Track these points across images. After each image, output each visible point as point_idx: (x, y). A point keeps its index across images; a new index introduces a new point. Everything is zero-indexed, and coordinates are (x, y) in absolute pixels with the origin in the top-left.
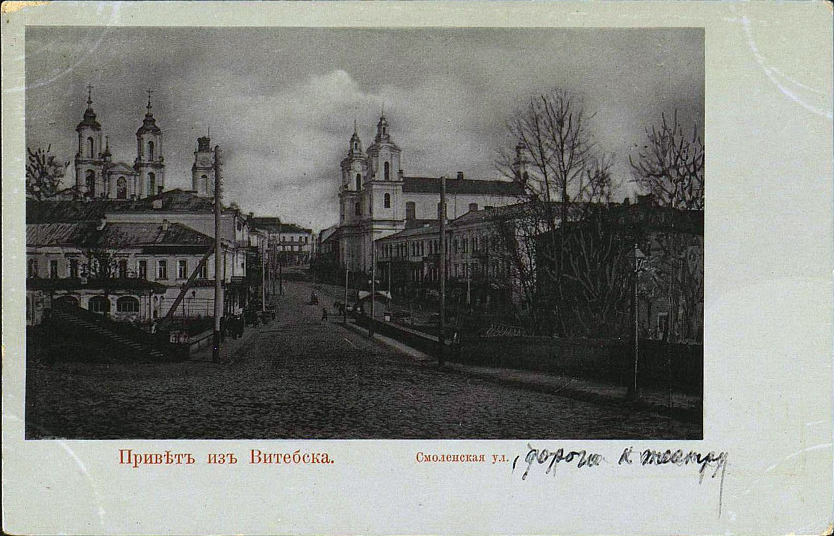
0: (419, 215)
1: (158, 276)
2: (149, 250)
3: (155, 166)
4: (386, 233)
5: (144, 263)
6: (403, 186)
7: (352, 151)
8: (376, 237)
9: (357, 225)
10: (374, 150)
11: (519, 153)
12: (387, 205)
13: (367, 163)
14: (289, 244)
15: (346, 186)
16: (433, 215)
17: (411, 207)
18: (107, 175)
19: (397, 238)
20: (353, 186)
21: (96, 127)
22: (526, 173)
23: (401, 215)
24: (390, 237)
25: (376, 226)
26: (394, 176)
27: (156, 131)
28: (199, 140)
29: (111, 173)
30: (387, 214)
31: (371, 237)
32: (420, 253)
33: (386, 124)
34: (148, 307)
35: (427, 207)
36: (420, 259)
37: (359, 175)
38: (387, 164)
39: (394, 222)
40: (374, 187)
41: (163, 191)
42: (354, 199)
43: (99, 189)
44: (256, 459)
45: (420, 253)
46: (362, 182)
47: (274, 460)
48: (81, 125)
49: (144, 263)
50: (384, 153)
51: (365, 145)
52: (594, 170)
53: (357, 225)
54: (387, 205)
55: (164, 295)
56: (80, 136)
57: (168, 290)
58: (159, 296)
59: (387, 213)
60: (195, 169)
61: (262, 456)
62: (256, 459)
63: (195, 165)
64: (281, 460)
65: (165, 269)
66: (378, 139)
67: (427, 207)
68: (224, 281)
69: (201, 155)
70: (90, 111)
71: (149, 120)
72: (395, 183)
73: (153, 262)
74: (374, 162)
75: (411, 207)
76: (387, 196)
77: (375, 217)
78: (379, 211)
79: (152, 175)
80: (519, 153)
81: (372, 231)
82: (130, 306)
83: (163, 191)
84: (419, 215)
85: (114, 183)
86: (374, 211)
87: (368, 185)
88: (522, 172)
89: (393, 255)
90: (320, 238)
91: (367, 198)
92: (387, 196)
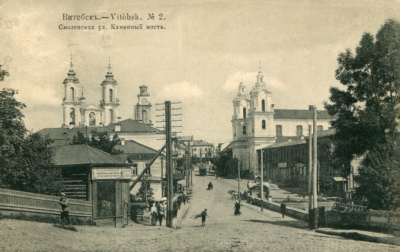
0: (285, 134)
3: (113, 105)
6: (274, 115)
9: (244, 138)
12: (264, 127)
13: (251, 102)
16: (293, 133)
17: (279, 127)
18: (83, 112)
20: (241, 116)
23: (274, 134)
26: (268, 108)
27: (114, 83)
29: (86, 110)
30: (265, 133)
35: (290, 129)
37: (244, 109)
38: (263, 101)
39: (269, 138)
43: (78, 119)
44: (65, 18)
46: (247, 112)
47: (73, 18)
51: (247, 91)
53: (244, 138)
54: (264, 127)
61: (67, 17)
62: (65, 18)
64: (76, 18)
65: (136, 169)
68: (162, 159)
72: (268, 114)
74: (255, 102)
75: (279, 127)
76: (264, 122)
78: (258, 132)
79: (111, 111)
84: (285, 134)
85: (87, 115)
86: (255, 131)
92: (264, 122)
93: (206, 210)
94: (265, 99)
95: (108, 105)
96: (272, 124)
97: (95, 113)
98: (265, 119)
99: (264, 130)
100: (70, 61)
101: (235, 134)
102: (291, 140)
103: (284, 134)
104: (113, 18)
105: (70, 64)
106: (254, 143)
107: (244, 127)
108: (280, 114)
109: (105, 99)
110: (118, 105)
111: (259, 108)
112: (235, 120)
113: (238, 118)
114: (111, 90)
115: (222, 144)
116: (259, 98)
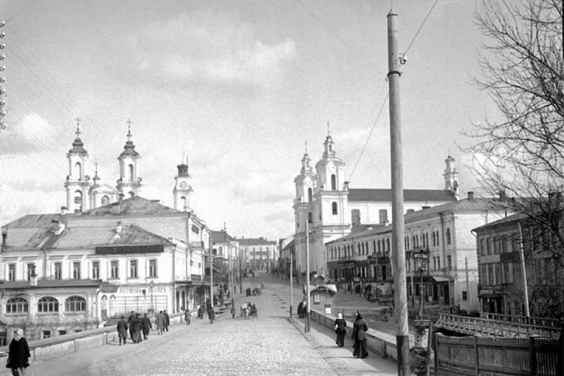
0: (363, 221)
1: (110, 276)
2: (102, 251)
4: (334, 238)
5: (96, 264)
7: (303, 168)
8: (326, 240)
10: (321, 165)
11: (448, 165)
12: (335, 211)
14: (258, 253)
15: (300, 199)
16: (375, 220)
17: (356, 214)
19: (345, 240)
21: (84, 153)
22: (455, 182)
23: (348, 220)
24: (337, 241)
25: (324, 231)
26: (340, 186)
27: (136, 155)
28: (179, 167)
29: (96, 192)
30: (335, 220)
31: (322, 242)
32: (365, 252)
33: (332, 142)
34: (94, 306)
36: (365, 258)
37: (310, 190)
38: (333, 177)
39: (341, 227)
40: (323, 197)
41: (124, 198)
42: (308, 213)
45: (365, 252)
48: (71, 151)
49: (96, 264)
50: (331, 168)
52: (548, 121)
54: (335, 211)
55: (116, 294)
56: (70, 161)
57: (119, 290)
58: (108, 295)
59: (336, 221)
60: (175, 191)
63: (175, 188)
65: (117, 269)
66: (325, 155)
67: (371, 214)
69: (180, 180)
70: (78, 140)
71: (129, 146)
72: (340, 193)
73: (105, 262)
75: (356, 214)
76: (334, 205)
77: (324, 224)
78: (328, 218)
80: (448, 165)
81: (322, 236)
82: (78, 305)
83: (124, 198)
84: (363, 221)
87: (318, 195)
88: (452, 181)
89: (341, 256)
90: (281, 246)
91: (317, 206)
92: (334, 205)
93: (191, 178)
94: (335, 174)
95: (127, 186)
96: (347, 208)
97: (109, 196)
98: (334, 201)
99: (335, 216)
100: (76, 128)
101: (298, 224)
102: (371, 228)
103: (363, 221)
104: (225, 223)
105: (76, 131)
106: (323, 233)
107: (310, 215)
108: (357, 195)
109: (123, 178)
110: (139, 185)
111: (328, 186)
112: (298, 205)
113: (302, 201)
114: (131, 166)
115: (284, 239)
116: (327, 171)
